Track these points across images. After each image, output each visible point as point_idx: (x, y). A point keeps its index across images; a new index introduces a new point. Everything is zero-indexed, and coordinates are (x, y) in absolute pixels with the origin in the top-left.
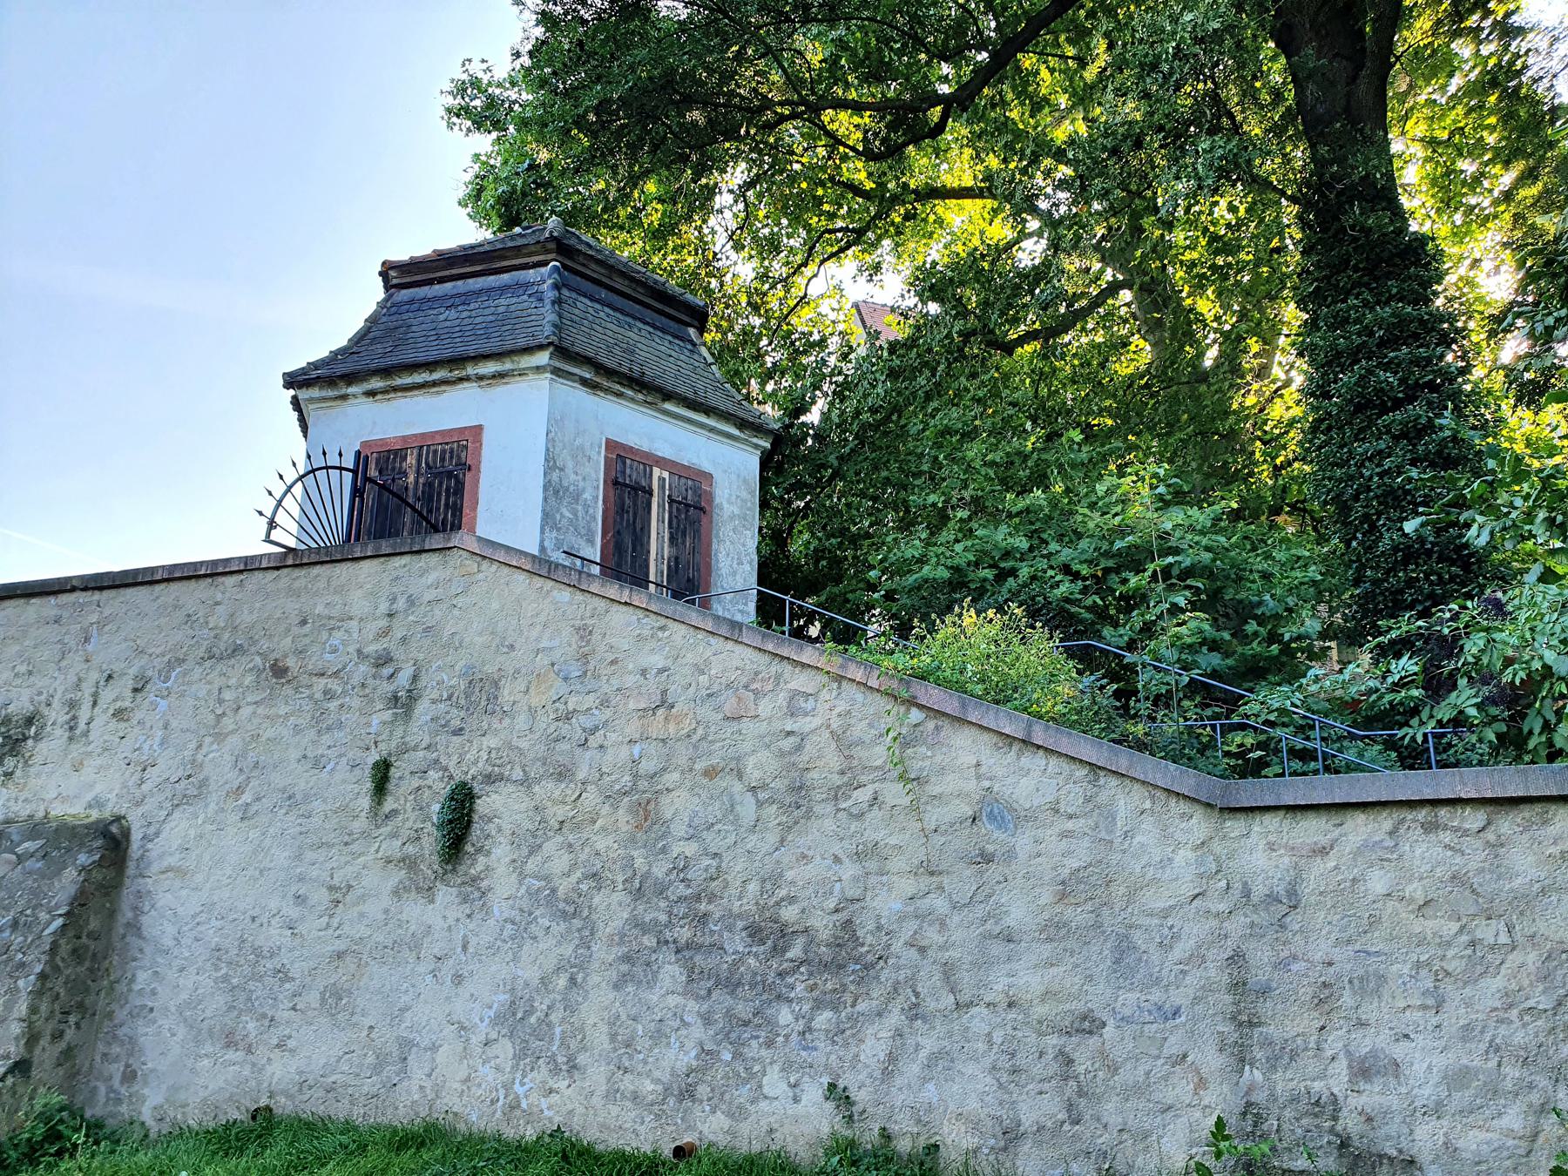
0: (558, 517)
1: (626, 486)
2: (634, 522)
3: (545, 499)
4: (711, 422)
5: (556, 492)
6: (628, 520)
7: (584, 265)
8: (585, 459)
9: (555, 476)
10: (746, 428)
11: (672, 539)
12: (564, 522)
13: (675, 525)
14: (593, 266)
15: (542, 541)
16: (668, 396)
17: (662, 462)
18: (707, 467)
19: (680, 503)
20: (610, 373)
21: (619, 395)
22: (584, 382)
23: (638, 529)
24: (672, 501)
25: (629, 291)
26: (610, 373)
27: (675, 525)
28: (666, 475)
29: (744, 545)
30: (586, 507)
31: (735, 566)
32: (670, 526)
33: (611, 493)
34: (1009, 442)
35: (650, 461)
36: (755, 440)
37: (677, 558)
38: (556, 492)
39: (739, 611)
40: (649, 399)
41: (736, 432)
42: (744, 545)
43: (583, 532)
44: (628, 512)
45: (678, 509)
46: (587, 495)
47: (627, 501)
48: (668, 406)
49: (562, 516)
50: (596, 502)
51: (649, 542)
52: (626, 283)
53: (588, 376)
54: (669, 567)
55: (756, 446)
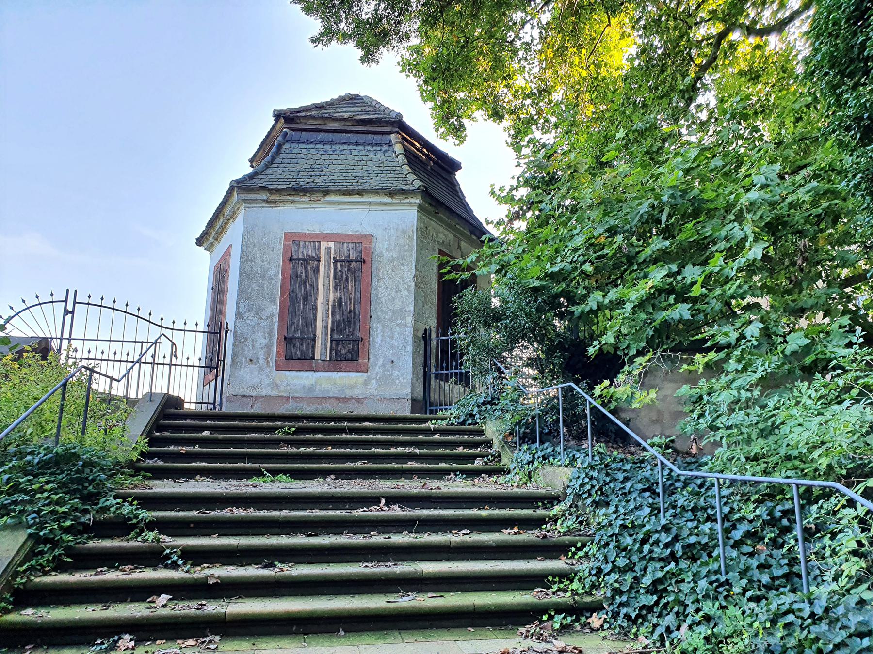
0: (249, 291)
1: (299, 259)
2: (305, 282)
3: (240, 282)
4: (340, 207)
5: (248, 276)
6: (301, 282)
7: (305, 123)
8: (270, 250)
9: (247, 266)
10: (396, 194)
11: (337, 287)
12: (253, 293)
13: (338, 276)
14: (312, 122)
15: (237, 308)
16: (326, 192)
17: (327, 237)
18: (368, 230)
19: (343, 261)
20: (278, 191)
21: (293, 202)
22: (267, 201)
23: (308, 286)
24: (336, 261)
25: (343, 128)
26: (278, 191)
27: (338, 276)
28: (332, 245)
29: (402, 278)
30: (270, 279)
31: (394, 294)
32: (335, 277)
33: (288, 267)
34: (759, 100)
35: (316, 239)
36: (407, 201)
37: (340, 299)
38: (248, 276)
39: (397, 325)
40: (313, 198)
41: (389, 200)
42: (402, 278)
43: (267, 296)
44: (300, 276)
45: (341, 265)
46: (271, 273)
47: (300, 269)
48: (328, 198)
49: (253, 290)
50: (278, 276)
51: (317, 293)
52: (319, 122)
53: (265, 197)
54: (334, 306)
55: (410, 204)
